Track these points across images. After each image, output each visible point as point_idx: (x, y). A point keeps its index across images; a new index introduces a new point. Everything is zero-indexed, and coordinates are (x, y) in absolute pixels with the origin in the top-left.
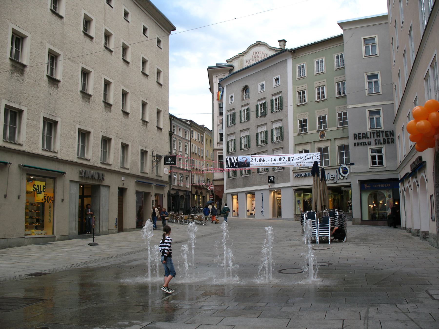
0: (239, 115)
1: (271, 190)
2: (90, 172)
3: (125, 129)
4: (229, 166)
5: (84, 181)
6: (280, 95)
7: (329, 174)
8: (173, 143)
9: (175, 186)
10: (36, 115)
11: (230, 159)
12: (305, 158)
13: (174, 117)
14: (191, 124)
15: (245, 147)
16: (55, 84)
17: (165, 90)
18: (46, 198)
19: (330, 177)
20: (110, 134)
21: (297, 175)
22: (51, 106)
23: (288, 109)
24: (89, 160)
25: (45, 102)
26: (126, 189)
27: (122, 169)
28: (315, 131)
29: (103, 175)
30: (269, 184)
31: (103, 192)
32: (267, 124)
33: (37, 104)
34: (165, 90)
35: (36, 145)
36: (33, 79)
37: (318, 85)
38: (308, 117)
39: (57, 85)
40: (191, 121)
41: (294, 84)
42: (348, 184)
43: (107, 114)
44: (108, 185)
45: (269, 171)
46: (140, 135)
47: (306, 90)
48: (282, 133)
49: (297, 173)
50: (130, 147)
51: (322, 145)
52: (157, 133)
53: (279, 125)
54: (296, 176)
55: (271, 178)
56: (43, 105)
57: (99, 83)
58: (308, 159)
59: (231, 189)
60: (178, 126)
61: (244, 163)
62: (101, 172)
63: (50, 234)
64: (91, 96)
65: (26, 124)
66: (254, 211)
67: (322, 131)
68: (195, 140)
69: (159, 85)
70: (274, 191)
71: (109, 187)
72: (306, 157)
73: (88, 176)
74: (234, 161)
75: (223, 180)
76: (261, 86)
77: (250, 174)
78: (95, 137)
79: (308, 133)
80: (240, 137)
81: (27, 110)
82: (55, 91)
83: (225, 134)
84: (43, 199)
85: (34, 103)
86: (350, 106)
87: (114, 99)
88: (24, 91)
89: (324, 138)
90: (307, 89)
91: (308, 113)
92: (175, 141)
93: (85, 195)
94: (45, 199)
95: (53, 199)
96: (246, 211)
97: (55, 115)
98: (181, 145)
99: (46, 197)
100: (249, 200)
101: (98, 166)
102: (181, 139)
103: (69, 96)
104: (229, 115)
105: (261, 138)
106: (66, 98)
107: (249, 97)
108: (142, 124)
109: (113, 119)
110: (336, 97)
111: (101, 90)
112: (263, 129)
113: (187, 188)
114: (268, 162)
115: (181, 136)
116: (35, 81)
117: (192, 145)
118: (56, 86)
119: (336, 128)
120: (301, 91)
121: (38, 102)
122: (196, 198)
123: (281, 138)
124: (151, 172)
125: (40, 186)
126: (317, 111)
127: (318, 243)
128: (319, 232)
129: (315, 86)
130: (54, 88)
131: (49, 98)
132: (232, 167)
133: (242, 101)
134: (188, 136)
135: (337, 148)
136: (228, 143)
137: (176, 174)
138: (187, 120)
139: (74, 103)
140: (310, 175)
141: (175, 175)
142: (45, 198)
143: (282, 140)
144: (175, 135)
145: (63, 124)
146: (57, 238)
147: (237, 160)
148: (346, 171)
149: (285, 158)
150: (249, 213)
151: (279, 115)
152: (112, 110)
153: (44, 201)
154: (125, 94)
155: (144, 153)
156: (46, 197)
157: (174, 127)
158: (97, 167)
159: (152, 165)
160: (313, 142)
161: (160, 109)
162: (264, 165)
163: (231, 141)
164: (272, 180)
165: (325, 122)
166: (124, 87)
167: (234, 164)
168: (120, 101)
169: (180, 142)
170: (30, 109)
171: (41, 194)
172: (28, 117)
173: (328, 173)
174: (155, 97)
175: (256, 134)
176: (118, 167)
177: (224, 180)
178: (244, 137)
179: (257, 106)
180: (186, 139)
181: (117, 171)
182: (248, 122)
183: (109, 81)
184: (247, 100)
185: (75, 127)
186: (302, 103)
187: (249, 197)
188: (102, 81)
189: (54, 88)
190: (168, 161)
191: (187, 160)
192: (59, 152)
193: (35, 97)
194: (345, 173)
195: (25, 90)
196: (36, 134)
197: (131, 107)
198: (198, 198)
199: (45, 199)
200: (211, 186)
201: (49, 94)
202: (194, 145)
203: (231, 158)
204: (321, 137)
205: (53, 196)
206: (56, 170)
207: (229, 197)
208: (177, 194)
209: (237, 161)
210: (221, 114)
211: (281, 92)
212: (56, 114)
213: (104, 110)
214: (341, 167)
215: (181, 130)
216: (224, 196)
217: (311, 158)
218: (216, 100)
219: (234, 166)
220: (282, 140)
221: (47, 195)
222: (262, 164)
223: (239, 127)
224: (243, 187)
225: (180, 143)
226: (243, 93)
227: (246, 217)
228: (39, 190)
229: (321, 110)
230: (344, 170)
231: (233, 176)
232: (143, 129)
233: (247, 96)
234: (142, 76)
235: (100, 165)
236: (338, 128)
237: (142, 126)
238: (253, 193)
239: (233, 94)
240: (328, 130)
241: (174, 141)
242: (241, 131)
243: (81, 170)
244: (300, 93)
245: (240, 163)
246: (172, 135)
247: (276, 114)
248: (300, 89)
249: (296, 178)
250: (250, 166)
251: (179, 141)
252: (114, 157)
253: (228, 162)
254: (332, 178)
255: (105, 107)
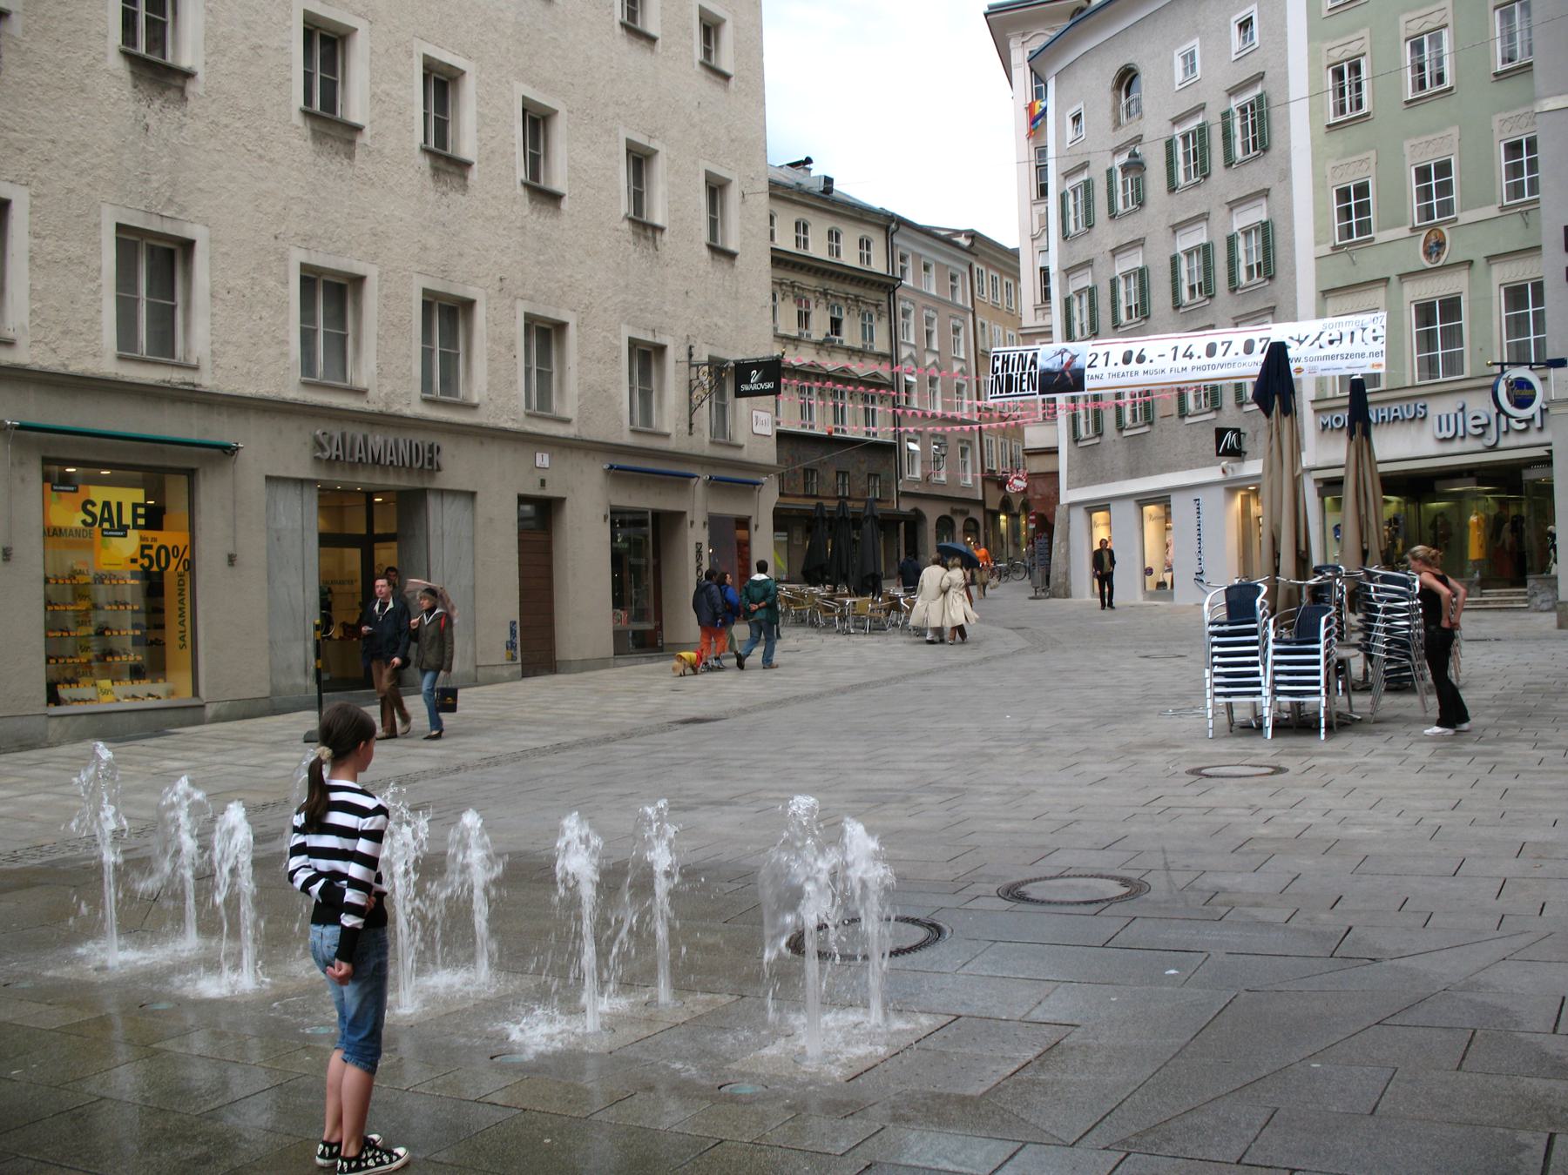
0: (1105, 186)
1: (1232, 487)
2: (365, 439)
3: (542, 258)
4: (1001, 392)
5: (340, 478)
6: (1258, 91)
7: (1462, 409)
8: (901, 319)
9: (916, 482)
10: (78, 216)
11: (1006, 362)
12: (1318, 338)
13: (902, 222)
14: (972, 245)
15: (1130, 317)
16: (169, 87)
17: (746, 95)
18: (153, 553)
19: (1470, 423)
20: (464, 283)
21: (1329, 418)
22: (154, 177)
23: (1290, 147)
24: (362, 392)
25: (119, 163)
26: (562, 500)
27: (535, 421)
28: (1404, 231)
29: (434, 450)
30: (1224, 463)
31: (442, 519)
32: (1211, 217)
33: (81, 173)
34: (746, 95)
35: (85, 340)
36: (47, 66)
37: (1415, 27)
38: (1372, 172)
39: (182, 90)
40: (973, 235)
41: (1313, 35)
42: (1541, 452)
43: (445, 200)
44: (464, 488)
45: (1224, 407)
46: (622, 283)
47: (1363, 55)
48: (1267, 248)
49: (1331, 413)
50: (572, 333)
51: (1434, 289)
52: (710, 269)
53: (1255, 214)
54: (1325, 426)
55: (1230, 438)
56: (110, 175)
57: (401, 77)
58: (1331, 342)
59: (1087, 488)
60: (920, 256)
61: (1062, 372)
62: (421, 438)
63: (185, 696)
64: (357, 129)
65: (26, 256)
66: (1170, 574)
67: (1434, 227)
68: (995, 307)
69: (713, 77)
70: (1245, 488)
71: (472, 495)
72: (1321, 333)
73: (357, 456)
74: (1024, 369)
75: (1054, 451)
76: (1185, 58)
77: (1151, 424)
78: (387, 296)
79: (1373, 239)
80: (1112, 277)
81: (27, 199)
82: (173, 114)
83: (1056, 268)
84: (138, 556)
85: (66, 167)
86: (1550, 104)
87: (480, 140)
88: (7, 118)
89: (1443, 258)
90: (1368, 55)
91: (1372, 154)
92: (909, 312)
93: (377, 531)
94: (149, 557)
95: (186, 556)
96: (1138, 572)
97: (177, 213)
98: (935, 328)
99: (150, 547)
100: (1151, 529)
101: (408, 412)
102: (935, 306)
103: (247, 132)
104: (1069, 191)
105: (1189, 273)
106: (229, 142)
107: (1139, 109)
108: (630, 236)
109: (480, 221)
110: (1496, 75)
111: (412, 104)
112: (1196, 237)
113: (964, 488)
114: (1159, 364)
115: (933, 292)
116: (58, 75)
117: (983, 325)
118: (171, 94)
119: (1493, 211)
120: (1343, 61)
121: (85, 165)
122: (1003, 524)
123: (1267, 268)
124: (686, 428)
125: (119, 505)
126: (1415, 142)
127: (1269, 736)
128: (1275, 683)
129: (1403, 36)
130: (166, 101)
131: (142, 144)
132: (1013, 393)
133: (1115, 129)
134: (964, 292)
135: (1499, 299)
136: (1067, 303)
137: (918, 438)
138: (958, 233)
139: (271, 161)
140: (1383, 418)
141: (914, 441)
142: (147, 552)
143: (1271, 278)
144: (908, 288)
145: (224, 250)
146: (210, 711)
147: (1033, 363)
148: (1526, 392)
149: (1230, 343)
150: (1151, 582)
151: (1255, 176)
152: (469, 182)
153: (142, 566)
154: (537, 122)
155: (646, 356)
156: (150, 547)
157: (903, 258)
158: (402, 417)
159: (690, 401)
160: (1394, 279)
161: (723, 173)
162: (1142, 379)
163: (1079, 293)
164: (1232, 445)
165: (1445, 188)
166: (530, 88)
167: (1022, 381)
168: (514, 145)
169: (931, 314)
170: (45, 196)
171: (125, 536)
172: (38, 229)
173: (1460, 406)
174: (693, 126)
175: (1168, 262)
176: (515, 414)
177: (1057, 452)
178: (1127, 277)
179: (1170, 145)
180: (953, 305)
181: (505, 431)
182: (1138, 214)
183: (450, 66)
184: (1134, 124)
185: (283, 259)
186: (1349, 115)
187: (1151, 516)
188: (412, 66)
189: (166, 101)
190: (749, 383)
191: (961, 381)
192: (206, 365)
193: (69, 143)
194: (1523, 402)
195: (10, 114)
196: (83, 297)
197: (572, 168)
198: (1012, 525)
199: (143, 556)
200: (1018, 478)
201: (139, 128)
202: (990, 327)
203: (1009, 356)
204: (1428, 254)
205: (187, 542)
206: (195, 435)
207: (1078, 516)
208: (841, 515)
209: (1035, 368)
210: (1043, 191)
211: (1260, 77)
212: (183, 209)
213: (430, 183)
214: (1505, 376)
215: (933, 270)
216: (1059, 514)
217: (1347, 339)
218: (1025, 138)
219: (1021, 390)
220: (1271, 278)
221: (155, 540)
222: (1137, 375)
223: (1107, 234)
224: (1126, 479)
225: (929, 321)
226: (1118, 99)
227: (1139, 599)
228: (112, 524)
229: (1430, 138)
230: (1517, 392)
231: (1091, 434)
232: (636, 256)
233: (1133, 107)
234: (625, 40)
235: (416, 409)
236: (1503, 208)
237: (632, 247)
238: (1162, 499)
239: (1081, 105)
240: (1459, 223)
241: (906, 313)
242: (1115, 252)
243: (318, 432)
244: (1339, 74)
245: (1047, 375)
246: (895, 289)
247: (1246, 170)
248: (1337, 55)
249: (1327, 431)
250: (1088, 384)
251: (925, 311)
252: (492, 372)
253: (1000, 373)
254: (1476, 426)
255: (436, 171)
